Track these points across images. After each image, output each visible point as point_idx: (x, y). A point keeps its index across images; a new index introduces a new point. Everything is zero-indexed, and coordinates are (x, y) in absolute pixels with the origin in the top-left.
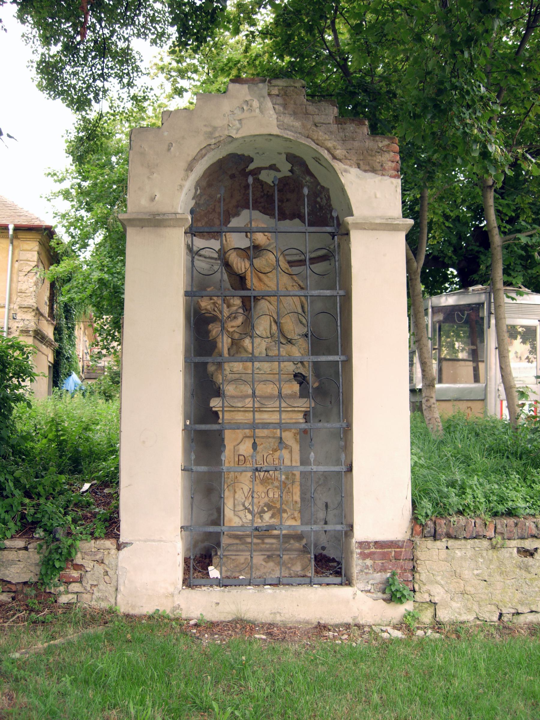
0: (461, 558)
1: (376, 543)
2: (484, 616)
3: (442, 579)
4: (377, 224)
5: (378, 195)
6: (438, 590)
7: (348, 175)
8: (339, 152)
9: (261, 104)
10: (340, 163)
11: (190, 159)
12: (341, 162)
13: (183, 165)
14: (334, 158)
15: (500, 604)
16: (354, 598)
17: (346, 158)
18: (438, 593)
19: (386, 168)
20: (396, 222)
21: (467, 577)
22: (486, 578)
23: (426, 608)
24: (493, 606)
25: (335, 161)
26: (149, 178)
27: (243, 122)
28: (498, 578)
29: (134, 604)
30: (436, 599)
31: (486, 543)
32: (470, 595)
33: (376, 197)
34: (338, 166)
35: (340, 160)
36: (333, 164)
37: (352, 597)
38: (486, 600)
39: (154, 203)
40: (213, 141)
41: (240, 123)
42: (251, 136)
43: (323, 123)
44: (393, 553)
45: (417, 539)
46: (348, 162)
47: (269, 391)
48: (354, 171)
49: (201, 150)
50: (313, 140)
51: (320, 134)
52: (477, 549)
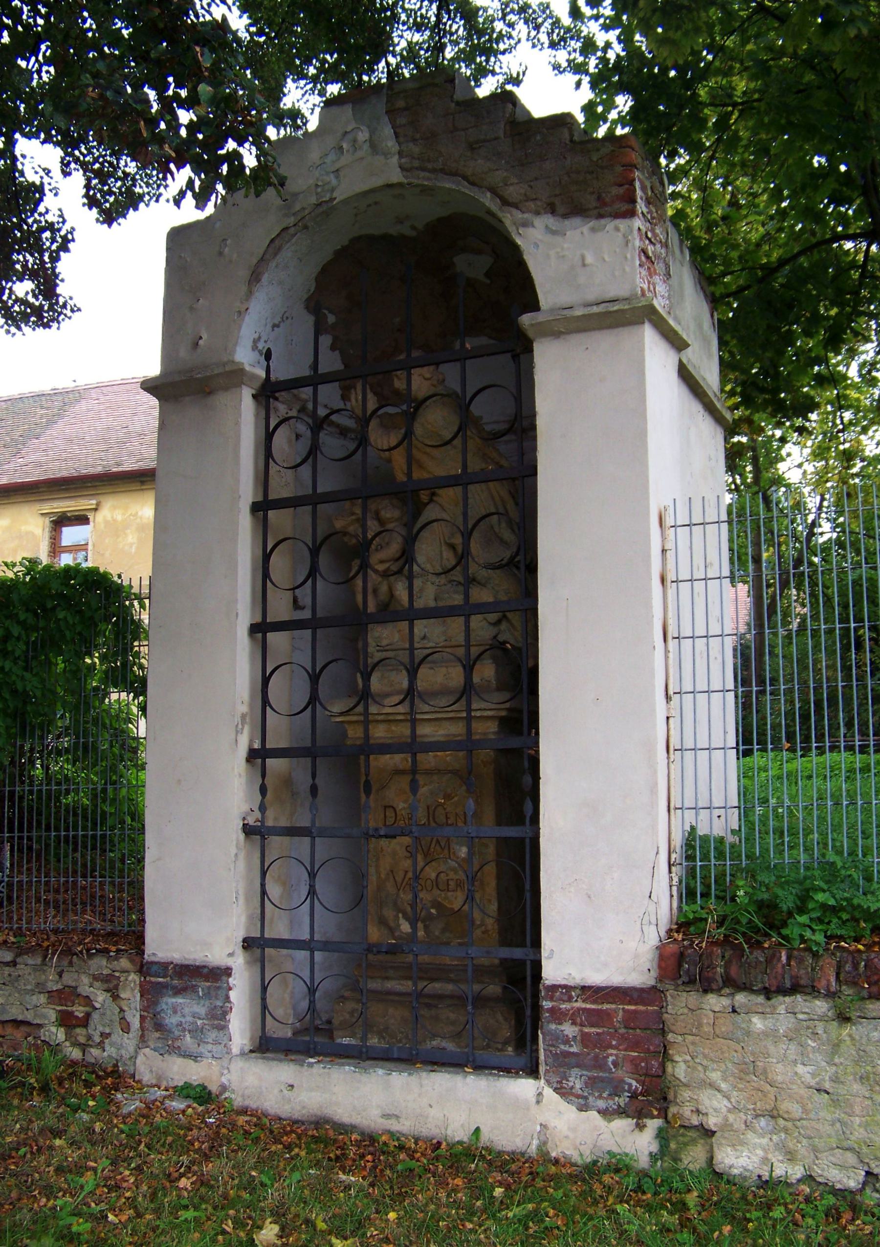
0: (765, 1034)
1: (584, 988)
2: (825, 1174)
3: (724, 1079)
4: (578, 317)
5: (589, 260)
6: (715, 1104)
7: (530, 231)
8: (513, 192)
9: (372, 132)
10: (515, 212)
11: (255, 261)
12: (517, 208)
13: (243, 273)
14: (506, 203)
15: (865, 1150)
16: (538, 1102)
17: (528, 199)
18: (715, 1110)
19: (607, 200)
20: (615, 308)
21: (779, 1078)
22: (827, 1085)
23: (694, 1141)
24: (849, 1154)
25: (506, 208)
26: (191, 308)
27: (342, 174)
28: (856, 1087)
29: (160, 1072)
30: (712, 1122)
31: (821, 1006)
32: (793, 1120)
33: (584, 265)
34: (509, 218)
35: (516, 206)
36: (500, 214)
37: (534, 1100)
38: (829, 1136)
39: (199, 351)
40: (292, 220)
41: (337, 177)
42: (357, 195)
43: (485, 141)
44: (621, 1013)
45: (669, 986)
46: (532, 205)
47: (440, 679)
48: (543, 222)
49: (272, 241)
50: (465, 178)
51: (478, 165)
52: (801, 1016)
